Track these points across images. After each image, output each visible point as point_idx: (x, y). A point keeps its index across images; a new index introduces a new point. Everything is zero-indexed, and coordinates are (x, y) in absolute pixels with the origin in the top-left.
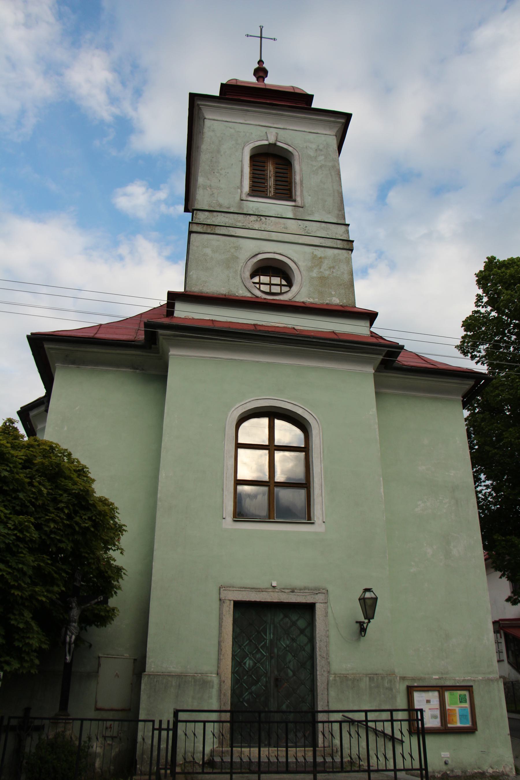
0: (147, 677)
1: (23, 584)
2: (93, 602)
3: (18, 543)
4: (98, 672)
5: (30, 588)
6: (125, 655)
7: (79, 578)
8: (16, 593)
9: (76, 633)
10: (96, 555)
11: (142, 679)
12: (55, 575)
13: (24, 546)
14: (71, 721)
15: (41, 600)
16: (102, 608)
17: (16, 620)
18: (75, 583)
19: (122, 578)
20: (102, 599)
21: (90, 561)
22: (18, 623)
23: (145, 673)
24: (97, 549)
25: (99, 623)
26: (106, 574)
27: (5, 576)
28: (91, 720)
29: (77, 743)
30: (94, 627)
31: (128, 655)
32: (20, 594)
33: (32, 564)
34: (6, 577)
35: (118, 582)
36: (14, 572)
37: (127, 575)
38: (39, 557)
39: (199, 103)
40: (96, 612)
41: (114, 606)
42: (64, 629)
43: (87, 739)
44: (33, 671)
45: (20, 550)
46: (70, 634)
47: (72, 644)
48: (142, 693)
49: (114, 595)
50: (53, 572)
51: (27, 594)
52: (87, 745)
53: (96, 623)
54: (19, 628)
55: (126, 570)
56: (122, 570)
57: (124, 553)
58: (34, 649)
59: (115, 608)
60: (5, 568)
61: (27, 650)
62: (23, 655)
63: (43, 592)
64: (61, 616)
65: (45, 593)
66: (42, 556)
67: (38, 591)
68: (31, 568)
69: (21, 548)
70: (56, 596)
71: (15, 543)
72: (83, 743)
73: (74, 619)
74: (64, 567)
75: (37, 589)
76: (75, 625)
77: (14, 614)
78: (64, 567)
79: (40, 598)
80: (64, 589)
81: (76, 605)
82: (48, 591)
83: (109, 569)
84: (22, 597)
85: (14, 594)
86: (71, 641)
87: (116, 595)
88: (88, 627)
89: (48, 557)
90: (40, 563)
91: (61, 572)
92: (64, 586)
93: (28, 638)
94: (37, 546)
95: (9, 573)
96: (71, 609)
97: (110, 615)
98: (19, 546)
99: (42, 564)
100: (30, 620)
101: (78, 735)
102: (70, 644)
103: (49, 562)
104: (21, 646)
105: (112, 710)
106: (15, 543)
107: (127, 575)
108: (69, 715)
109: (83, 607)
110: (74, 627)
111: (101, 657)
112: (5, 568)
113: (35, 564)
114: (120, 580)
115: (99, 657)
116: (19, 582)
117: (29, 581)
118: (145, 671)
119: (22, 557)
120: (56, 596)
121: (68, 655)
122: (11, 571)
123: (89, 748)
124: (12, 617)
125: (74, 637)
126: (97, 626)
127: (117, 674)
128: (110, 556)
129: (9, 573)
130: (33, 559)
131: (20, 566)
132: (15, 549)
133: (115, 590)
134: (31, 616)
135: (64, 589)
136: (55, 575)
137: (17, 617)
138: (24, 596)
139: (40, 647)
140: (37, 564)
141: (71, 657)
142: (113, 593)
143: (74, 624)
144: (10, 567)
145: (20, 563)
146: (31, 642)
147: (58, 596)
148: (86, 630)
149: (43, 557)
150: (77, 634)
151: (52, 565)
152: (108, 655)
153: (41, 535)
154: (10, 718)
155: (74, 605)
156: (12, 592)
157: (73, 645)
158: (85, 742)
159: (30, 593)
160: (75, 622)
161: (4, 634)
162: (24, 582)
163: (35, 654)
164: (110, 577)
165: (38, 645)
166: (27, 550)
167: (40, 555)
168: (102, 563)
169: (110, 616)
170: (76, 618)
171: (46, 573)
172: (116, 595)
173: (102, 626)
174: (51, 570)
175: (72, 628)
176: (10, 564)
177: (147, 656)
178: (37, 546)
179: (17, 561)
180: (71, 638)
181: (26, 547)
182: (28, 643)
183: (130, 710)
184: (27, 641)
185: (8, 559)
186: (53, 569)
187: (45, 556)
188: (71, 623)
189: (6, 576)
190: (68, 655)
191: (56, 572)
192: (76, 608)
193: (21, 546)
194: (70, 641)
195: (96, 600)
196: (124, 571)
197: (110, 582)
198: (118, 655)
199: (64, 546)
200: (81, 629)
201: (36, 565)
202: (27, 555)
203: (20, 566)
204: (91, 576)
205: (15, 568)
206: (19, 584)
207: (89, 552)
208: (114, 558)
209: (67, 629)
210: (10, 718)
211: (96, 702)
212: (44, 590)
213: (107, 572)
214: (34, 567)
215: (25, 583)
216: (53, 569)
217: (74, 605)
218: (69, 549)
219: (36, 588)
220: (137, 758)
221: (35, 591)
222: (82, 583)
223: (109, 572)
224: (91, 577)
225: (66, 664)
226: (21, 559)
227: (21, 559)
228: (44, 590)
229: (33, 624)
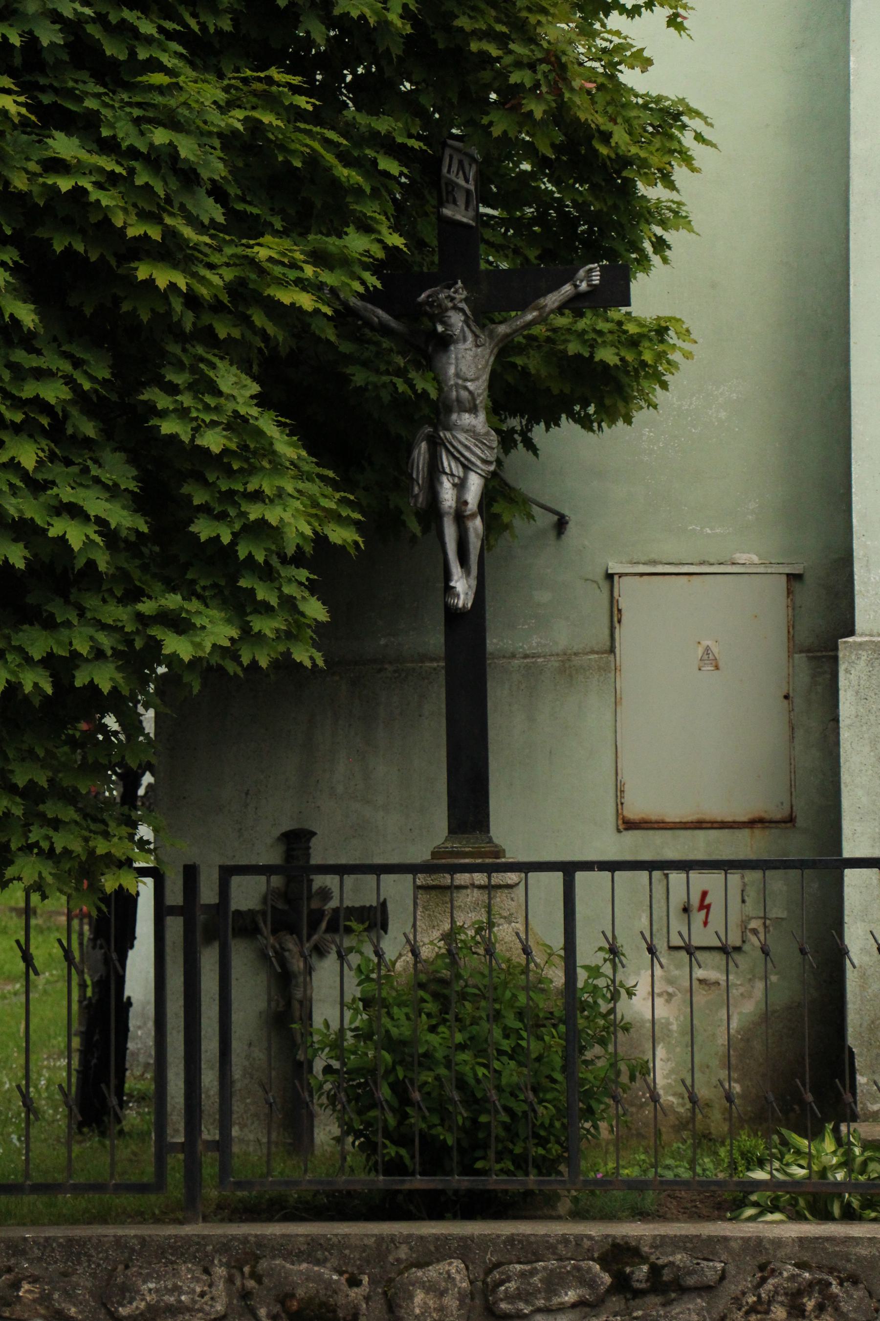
0: (864, 656)
1: (188, 232)
2: (552, 300)
3: (130, 16)
4: (612, 650)
5: (229, 251)
6: (741, 557)
7: (467, 180)
8: (163, 277)
9: (485, 462)
10: (545, 45)
11: (842, 668)
12: (343, 172)
13: (161, 29)
14: (512, 877)
15: (293, 304)
16: (602, 325)
17: (183, 413)
18: (447, 212)
19: (687, 159)
20: (596, 280)
21: (515, 78)
22: (196, 430)
23: (850, 639)
24: (544, 11)
25: (591, 409)
26: (604, 150)
27: (93, 198)
28: (612, 866)
29: (557, 977)
30: (567, 427)
31: (755, 559)
32: (182, 282)
33: (219, 121)
34: (98, 201)
35: (671, 185)
36: (132, 171)
37: (713, 145)
38: (245, 81)
39: (260, 1268)
40: (573, 348)
41: (665, 312)
42: (424, 445)
43: (598, 959)
44: (303, 655)
45: (143, 55)
46: (458, 471)
47: (473, 516)
48: (845, 735)
49: (656, 260)
50: (330, 158)
51: (216, 280)
52: (601, 982)
53: (577, 408)
54: (205, 452)
55: (705, 119)
56: (685, 119)
57: (686, 24)
58: (290, 551)
59: (670, 319)
60: (84, 155)
61: (260, 558)
62: (243, 583)
63: (294, 265)
64: (402, 387)
65: (309, 271)
66: (262, 75)
67: (270, 259)
68: (217, 143)
69: (148, 40)
70: (363, 283)
71: (113, 18)
72: (582, 976)
73: (464, 394)
74: (383, 125)
75: (263, 253)
76: (478, 421)
77: (172, 390)
78: (383, 125)
79: (286, 297)
80: (396, 240)
81: (466, 322)
82: (319, 258)
83: (613, 120)
84: (192, 300)
85: (150, 282)
86: (466, 503)
87: (665, 260)
88: (538, 433)
89: (296, 80)
90: (256, 114)
91: (370, 153)
92: (396, 228)
93: (257, 496)
94: (226, 25)
95: (110, 180)
96: (445, 342)
97: (648, 357)
98: (134, 30)
99: (267, 118)
100: (254, 411)
101: (557, 942)
102: (460, 518)
103: (303, 102)
104: (226, 539)
105: (699, 825)
106: (113, 18)
107: (713, 145)
108: (498, 853)
109: (502, 329)
110: (471, 431)
111: (621, 575)
112: (84, 155)
113: (236, 119)
114: (680, 173)
115: (610, 577)
116: (168, 221)
117: (218, 214)
118: (852, 633)
119: (161, 89)
120: (363, 283)
121: (456, 570)
122: (118, 170)
123: (615, 997)
124: (163, 401)
125: (475, 484)
126: (586, 423)
127: (707, 649)
128: (616, 40)
129: (110, 180)
130: (221, 96)
131: (160, 136)
132: (112, 49)
133: (658, 230)
134: (255, 388)
135: (396, 240)
136: (343, 172)
137: (186, 400)
138: (204, 291)
139: (320, 540)
140: (246, 120)
141: (474, 583)
142: (647, 246)
143: (467, 419)
144: (109, 146)
145: (156, 122)
146: (273, 516)
147: (372, 280)
148: (530, 446)
149: (270, 80)
150: (492, 468)
151: (316, 117)
152: (654, 563)
153: (622, 354)
154: (227, 872)
155: (457, 320)
156: (143, 273)
157: (477, 525)
158: (594, 971)
159: (229, 275)
160: (473, 410)
161: (132, 486)
162: (193, 221)
163: (303, 574)
164: (625, 162)
165: (308, 531)
166: (181, 49)
167: (249, 73)
168: (576, 84)
169: (644, 364)
170: (479, 387)
171: (298, 164)
172: (665, 260)
173: (612, 422)
174: (316, 145)
175: (462, 437)
176: (105, 133)
177: (858, 552)
178: (226, 25)
179: (137, 112)
180: (461, 486)
181: (170, 36)
182: (262, 523)
183: (790, 820)
184: (254, 512)
185: (91, 104)
186: (326, 142)
187: (274, 73)
188: (454, 416)
189: (95, 195)
190: (456, 570)
191: (345, 159)
192: (470, 338)
193: (147, 28)
194: (462, 503)
195: (567, 288)
196: (695, 124)
197: (627, 189)
198: (702, 563)
199: (368, 13)
200: (507, 441)
201: (240, 126)
202: (182, 78)
203: (160, 136)
204: (526, 166)
205: (133, 153)
206: (170, 233)
207: (501, 28)
208: (642, 50)
209: (435, 444)
210: (227, 872)
211: (619, 791)
212: (299, 256)
213: (606, 137)
214: (228, 139)
215: (201, 227)
216: (326, 142)
217: (457, 320)
218: (398, 23)
219: (256, 249)
220: (851, 1041)
221: (252, 262)
222: (483, 210)
223: (620, 136)
224: (525, 172)
225: (453, 616)
226: (158, 99)
227: (158, 99)
228: (299, 256)
229: (268, 424)
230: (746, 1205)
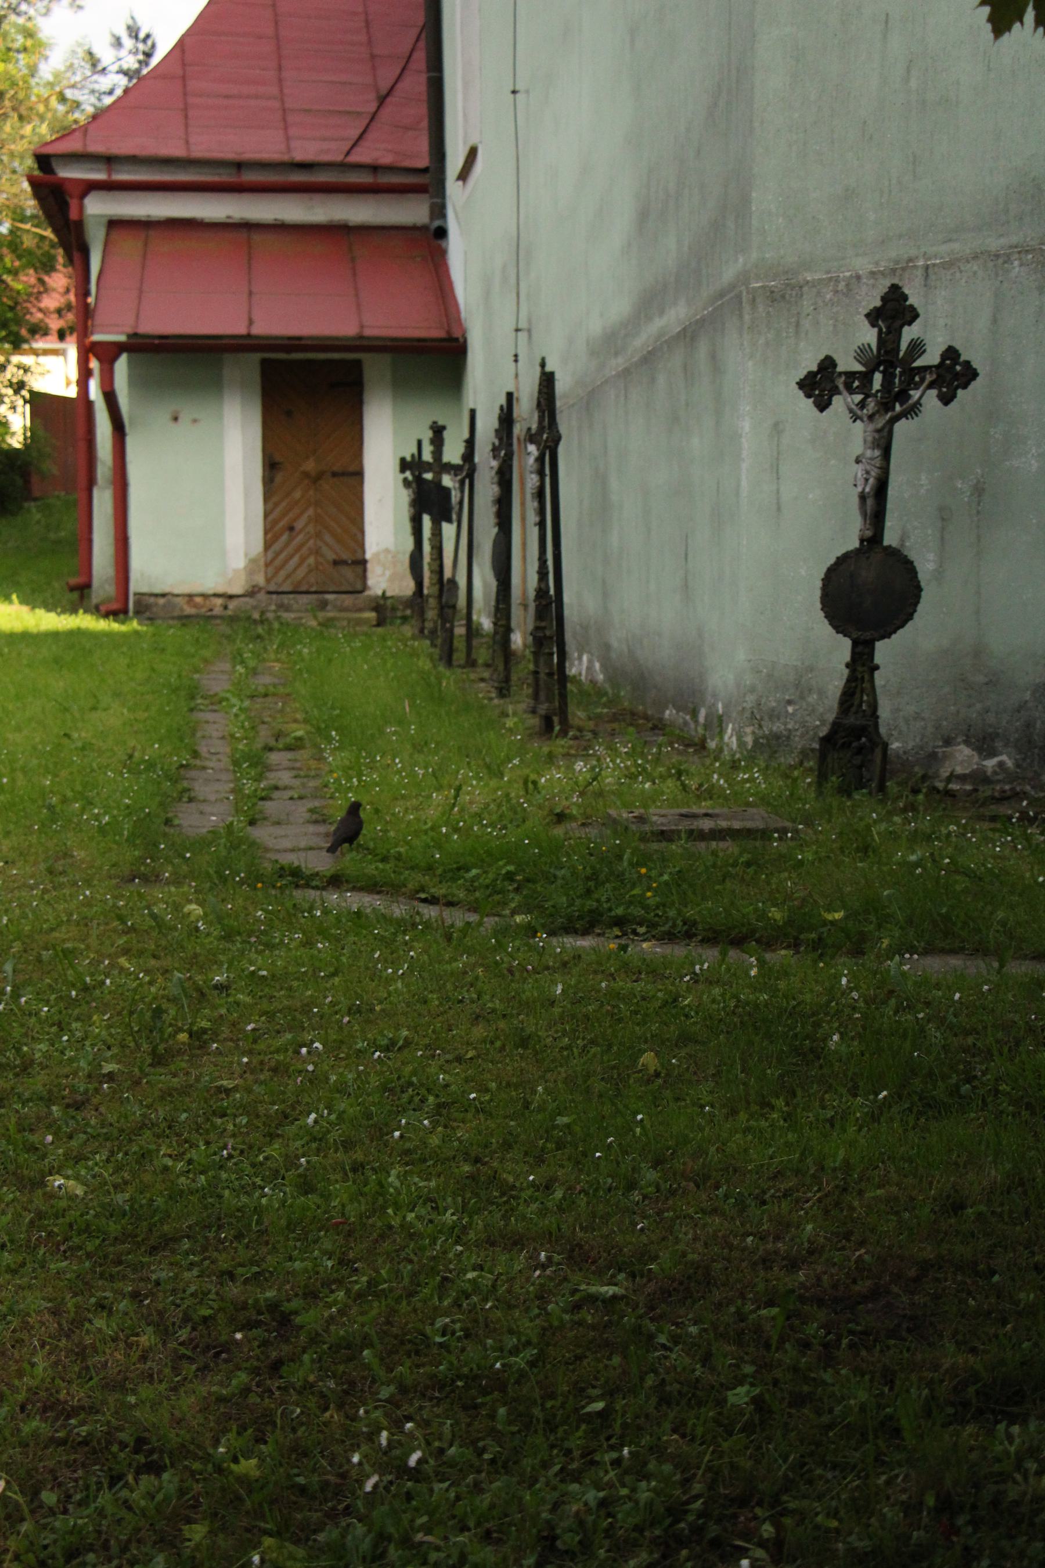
230: (937, 367)
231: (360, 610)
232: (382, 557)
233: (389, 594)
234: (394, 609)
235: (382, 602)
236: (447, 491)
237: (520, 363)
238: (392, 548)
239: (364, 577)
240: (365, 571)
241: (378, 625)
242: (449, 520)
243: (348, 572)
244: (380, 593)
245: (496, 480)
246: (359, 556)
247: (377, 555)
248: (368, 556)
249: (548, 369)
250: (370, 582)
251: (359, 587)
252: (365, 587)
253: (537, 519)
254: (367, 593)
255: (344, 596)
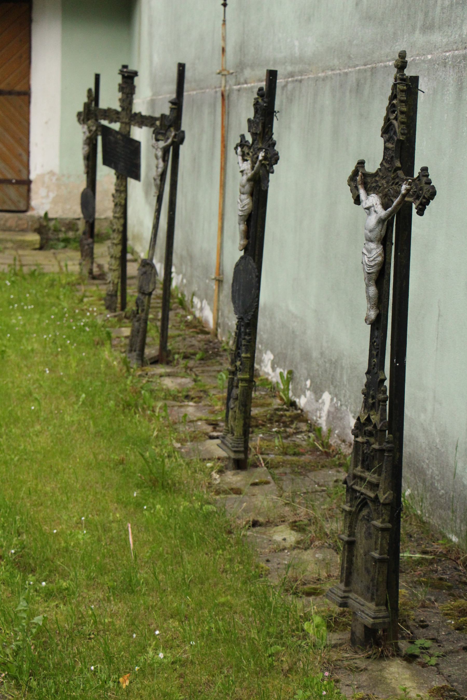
231: (24, 231)
232: (47, 179)
233: (50, 216)
234: (57, 230)
235: (45, 224)
236: (137, 145)
237: (227, 8)
238: (57, 170)
239: (28, 198)
240: (29, 190)
241: (41, 248)
242: (137, 177)
243: (12, 191)
244: (42, 214)
245: (247, 188)
246: (24, 177)
247: (42, 176)
248: (32, 176)
249: (408, 72)
250: (33, 203)
251: (22, 206)
252: (28, 207)
253: (373, 314)
254: (29, 213)
255: (8, 215)
